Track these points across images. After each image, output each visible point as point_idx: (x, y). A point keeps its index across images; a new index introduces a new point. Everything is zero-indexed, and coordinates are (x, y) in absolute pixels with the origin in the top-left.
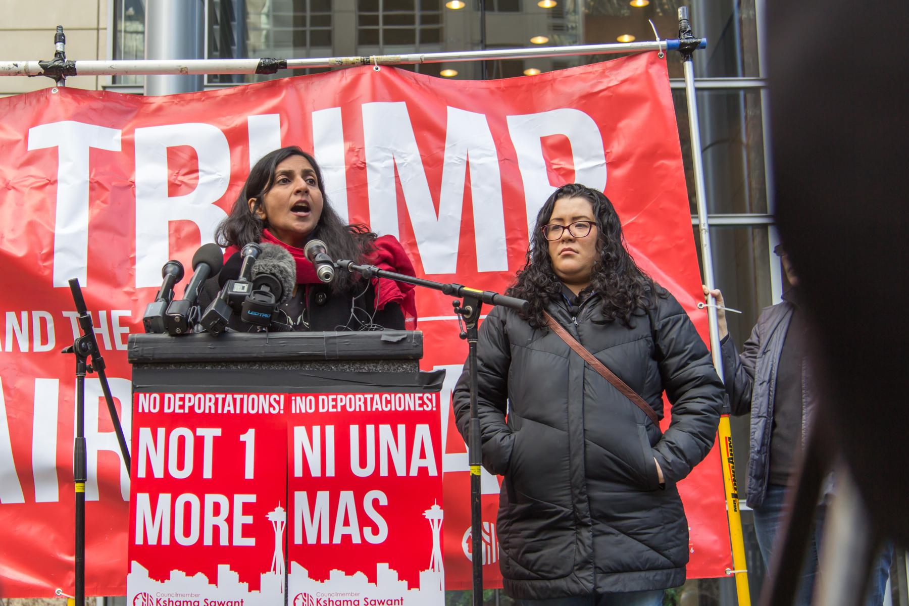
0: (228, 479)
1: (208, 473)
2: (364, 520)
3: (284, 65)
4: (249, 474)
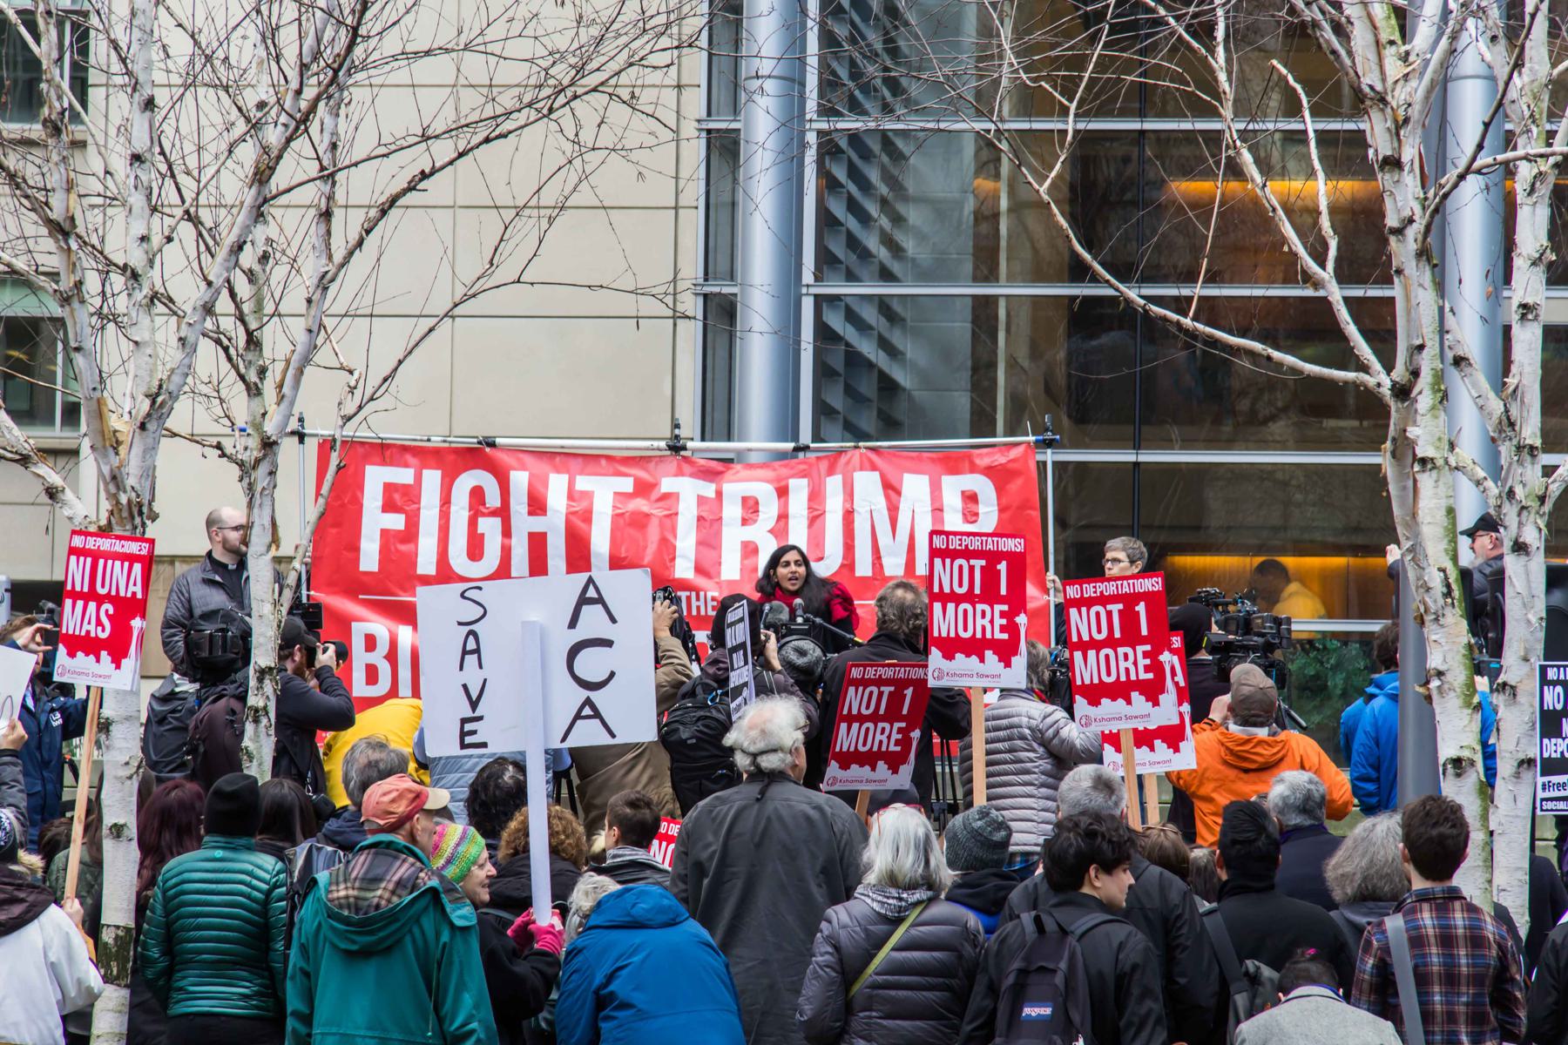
0: (1131, 637)
1: (1117, 635)
2: (99, 623)
4: (1144, 632)
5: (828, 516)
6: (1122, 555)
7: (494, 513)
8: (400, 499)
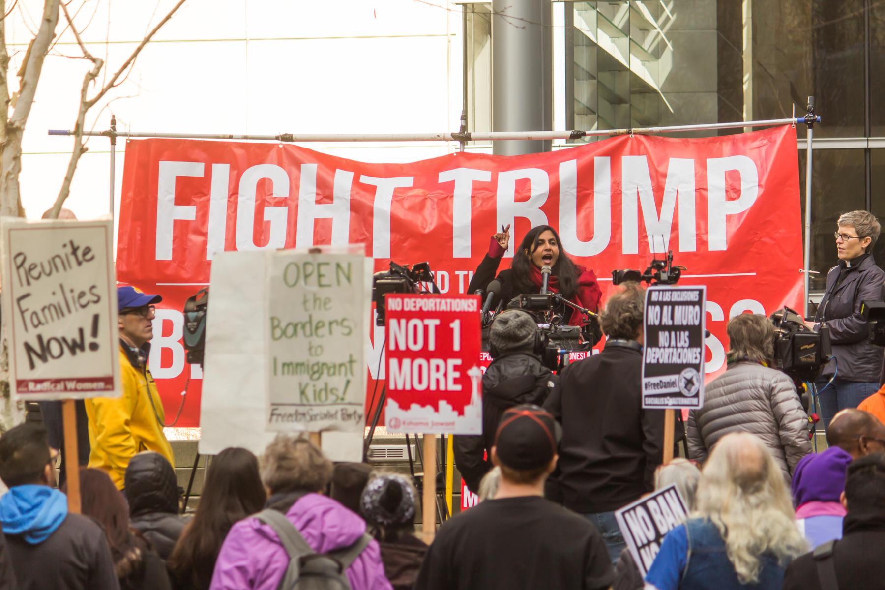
0: (444, 350)
1: (432, 347)
3: (584, 134)
4: (457, 347)
5: (596, 196)
6: (851, 231)
7: (280, 202)
8: (191, 191)
